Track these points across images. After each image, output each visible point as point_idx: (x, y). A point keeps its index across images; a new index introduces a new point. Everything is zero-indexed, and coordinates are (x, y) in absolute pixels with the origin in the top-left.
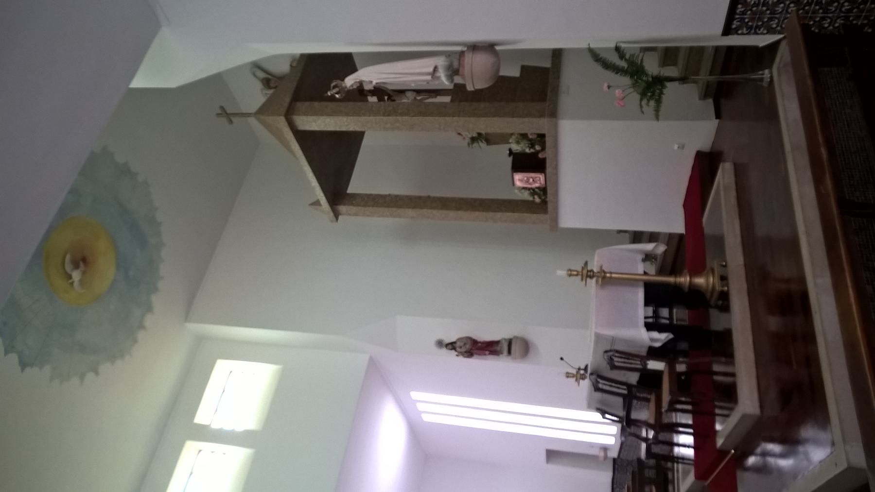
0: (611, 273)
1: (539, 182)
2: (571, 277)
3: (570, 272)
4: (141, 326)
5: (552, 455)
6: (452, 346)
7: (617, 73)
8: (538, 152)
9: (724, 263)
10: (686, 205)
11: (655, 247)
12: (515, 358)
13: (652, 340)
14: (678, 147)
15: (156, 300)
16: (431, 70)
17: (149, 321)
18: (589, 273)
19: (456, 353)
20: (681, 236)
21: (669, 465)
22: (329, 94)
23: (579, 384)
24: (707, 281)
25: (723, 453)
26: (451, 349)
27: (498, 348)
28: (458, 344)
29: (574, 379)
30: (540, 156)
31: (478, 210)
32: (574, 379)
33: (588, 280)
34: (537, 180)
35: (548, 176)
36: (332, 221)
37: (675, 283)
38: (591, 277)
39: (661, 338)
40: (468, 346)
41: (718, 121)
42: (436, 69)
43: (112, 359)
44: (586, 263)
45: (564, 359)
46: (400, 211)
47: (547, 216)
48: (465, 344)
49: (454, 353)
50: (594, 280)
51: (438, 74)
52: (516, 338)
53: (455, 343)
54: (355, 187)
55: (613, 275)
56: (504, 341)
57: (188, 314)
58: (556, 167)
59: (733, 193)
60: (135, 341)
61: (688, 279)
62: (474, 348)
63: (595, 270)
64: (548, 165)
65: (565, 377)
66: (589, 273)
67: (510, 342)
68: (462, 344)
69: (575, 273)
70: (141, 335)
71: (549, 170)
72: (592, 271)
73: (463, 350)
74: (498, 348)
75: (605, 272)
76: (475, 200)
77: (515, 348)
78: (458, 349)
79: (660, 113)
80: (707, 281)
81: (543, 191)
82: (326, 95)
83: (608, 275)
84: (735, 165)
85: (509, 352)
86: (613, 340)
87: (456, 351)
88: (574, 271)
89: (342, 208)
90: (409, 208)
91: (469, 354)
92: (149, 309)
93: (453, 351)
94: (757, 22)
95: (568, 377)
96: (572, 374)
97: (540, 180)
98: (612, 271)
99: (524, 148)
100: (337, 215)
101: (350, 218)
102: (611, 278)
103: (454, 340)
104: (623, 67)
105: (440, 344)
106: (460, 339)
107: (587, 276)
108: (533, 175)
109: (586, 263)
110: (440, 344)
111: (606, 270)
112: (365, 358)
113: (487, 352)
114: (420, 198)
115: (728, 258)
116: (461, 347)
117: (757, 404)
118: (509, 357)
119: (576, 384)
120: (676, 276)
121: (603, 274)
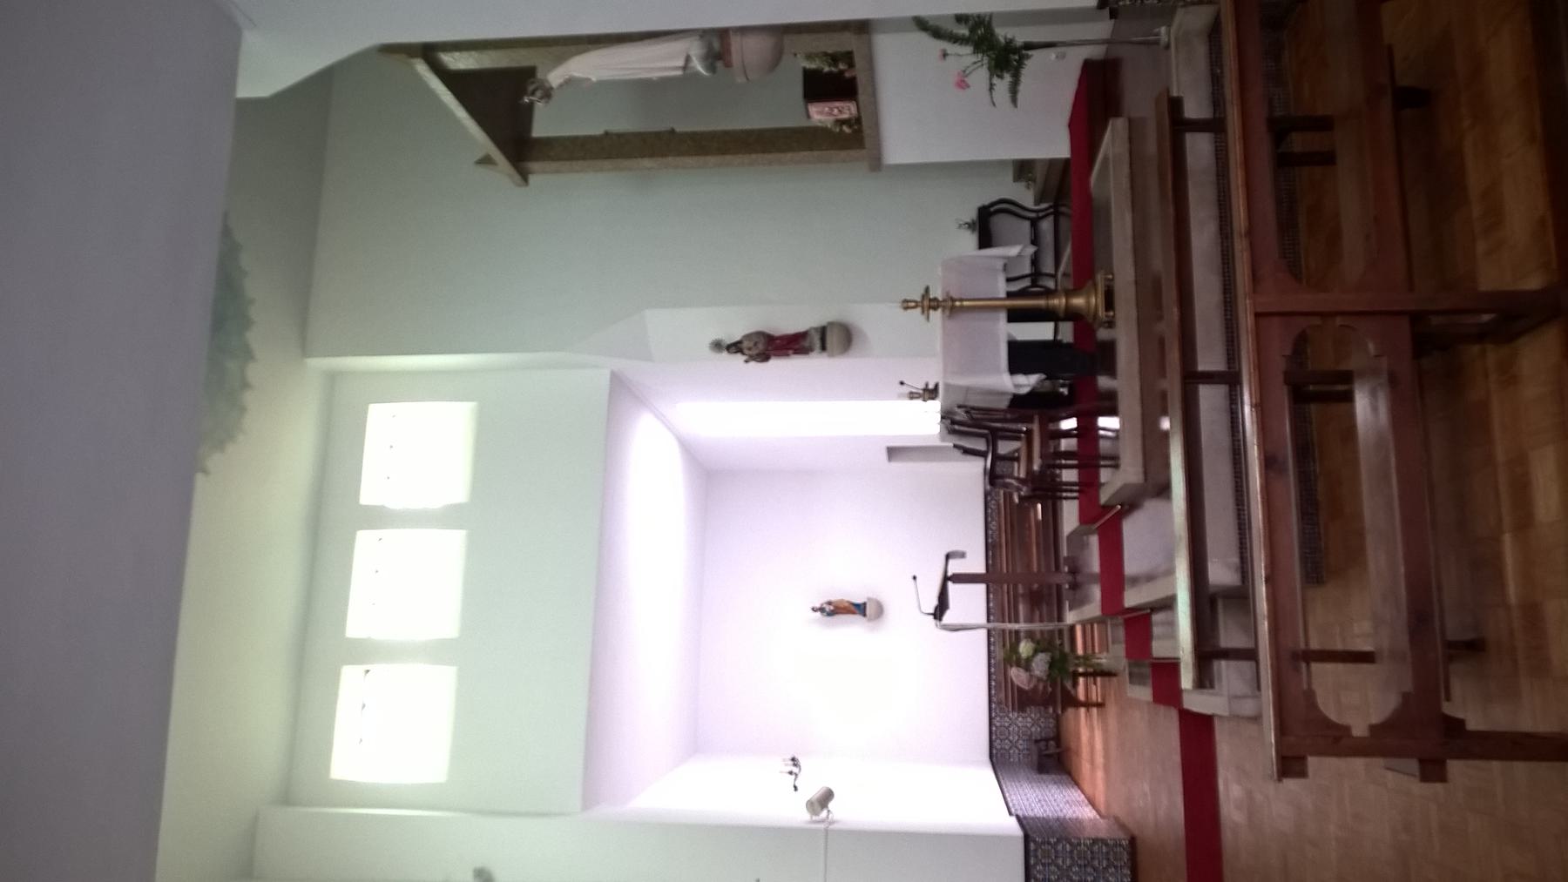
0: (961, 300)
1: (848, 112)
2: (909, 311)
3: (905, 305)
4: (245, 385)
5: (893, 452)
6: (735, 348)
7: (954, 42)
8: (842, 72)
9: (1110, 277)
10: (1072, 125)
11: (1022, 250)
12: (831, 355)
13: (1016, 386)
14: (1057, 57)
15: (253, 337)
16: (681, 63)
17: (254, 372)
18: (932, 304)
19: (745, 358)
20: (1067, 161)
21: (1058, 471)
22: (527, 101)
23: (928, 318)
24: (1088, 303)
25: (1107, 508)
26: (736, 352)
27: (806, 344)
28: (746, 344)
29: (919, 310)
30: (847, 75)
31: (756, 152)
32: (919, 310)
33: (931, 312)
34: (847, 110)
35: (861, 104)
36: (520, 186)
37: (1048, 305)
38: (935, 308)
39: (1027, 382)
40: (761, 347)
41: (1113, 21)
42: (688, 59)
43: (220, 445)
44: (927, 290)
45: (906, 382)
46: (627, 163)
47: (864, 152)
48: (755, 344)
49: (740, 358)
50: (940, 310)
51: (691, 65)
52: (831, 324)
53: (740, 342)
54: (545, 124)
55: (965, 303)
56: (813, 332)
57: (305, 348)
58: (874, 94)
59: (1126, 170)
60: (243, 410)
61: (1064, 301)
62: (770, 348)
63: (940, 299)
64: (860, 90)
65: (902, 310)
66: (932, 304)
67: (823, 331)
68: (751, 344)
69: (913, 304)
70: (249, 398)
71: (862, 97)
72: (935, 299)
73: (754, 352)
74: (806, 344)
75: (953, 300)
76: (749, 133)
77: (832, 339)
78: (746, 352)
79: (1020, 96)
80: (1088, 303)
81: (857, 121)
82: (521, 102)
83: (958, 303)
84: (1130, 121)
85: (824, 348)
86: (968, 389)
87: (743, 354)
88: (911, 301)
89: (534, 166)
90: (643, 156)
91: (764, 357)
92: (247, 355)
93: (739, 355)
94: (1030, 635)
95: (906, 308)
96: (916, 393)
97: (849, 109)
98: (963, 297)
99: (822, 66)
100: (524, 176)
101: (544, 178)
102: (962, 307)
103: (738, 338)
104: (964, 35)
105: (717, 346)
106: (748, 337)
107: (930, 307)
108: (837, 104)
109: (927, 290)
110: (717, 346)
111: (955, 296)
112: (603, 378)
113: (791, 352)
114: (658, 135)
115: (1115, 271)
116: (750, 349)
117: (1140, 469)
118: (825, 354)
119: (922, 318)
120: (1047, 298)
121: (950, 303)
